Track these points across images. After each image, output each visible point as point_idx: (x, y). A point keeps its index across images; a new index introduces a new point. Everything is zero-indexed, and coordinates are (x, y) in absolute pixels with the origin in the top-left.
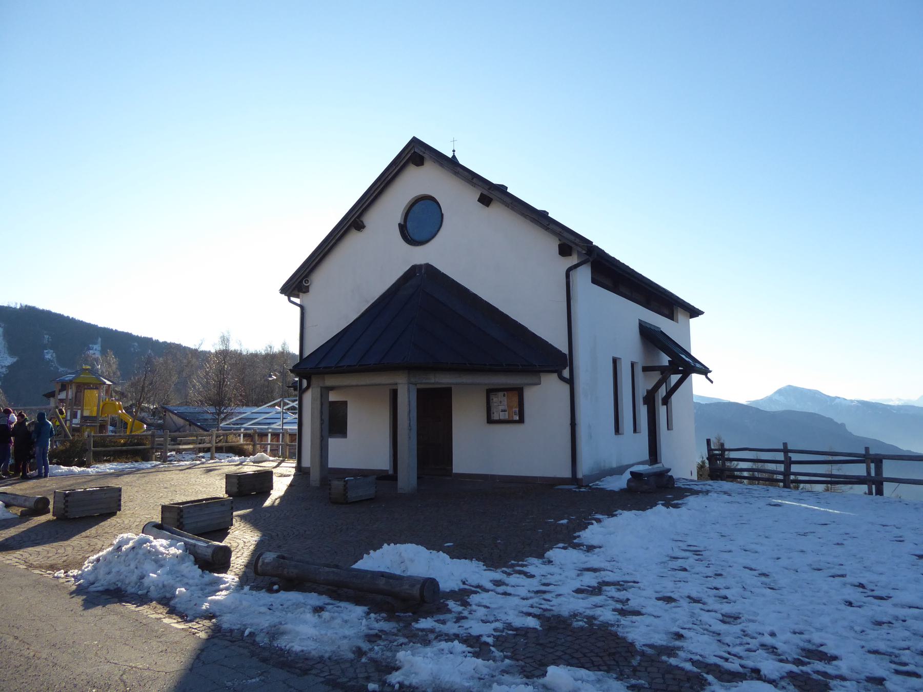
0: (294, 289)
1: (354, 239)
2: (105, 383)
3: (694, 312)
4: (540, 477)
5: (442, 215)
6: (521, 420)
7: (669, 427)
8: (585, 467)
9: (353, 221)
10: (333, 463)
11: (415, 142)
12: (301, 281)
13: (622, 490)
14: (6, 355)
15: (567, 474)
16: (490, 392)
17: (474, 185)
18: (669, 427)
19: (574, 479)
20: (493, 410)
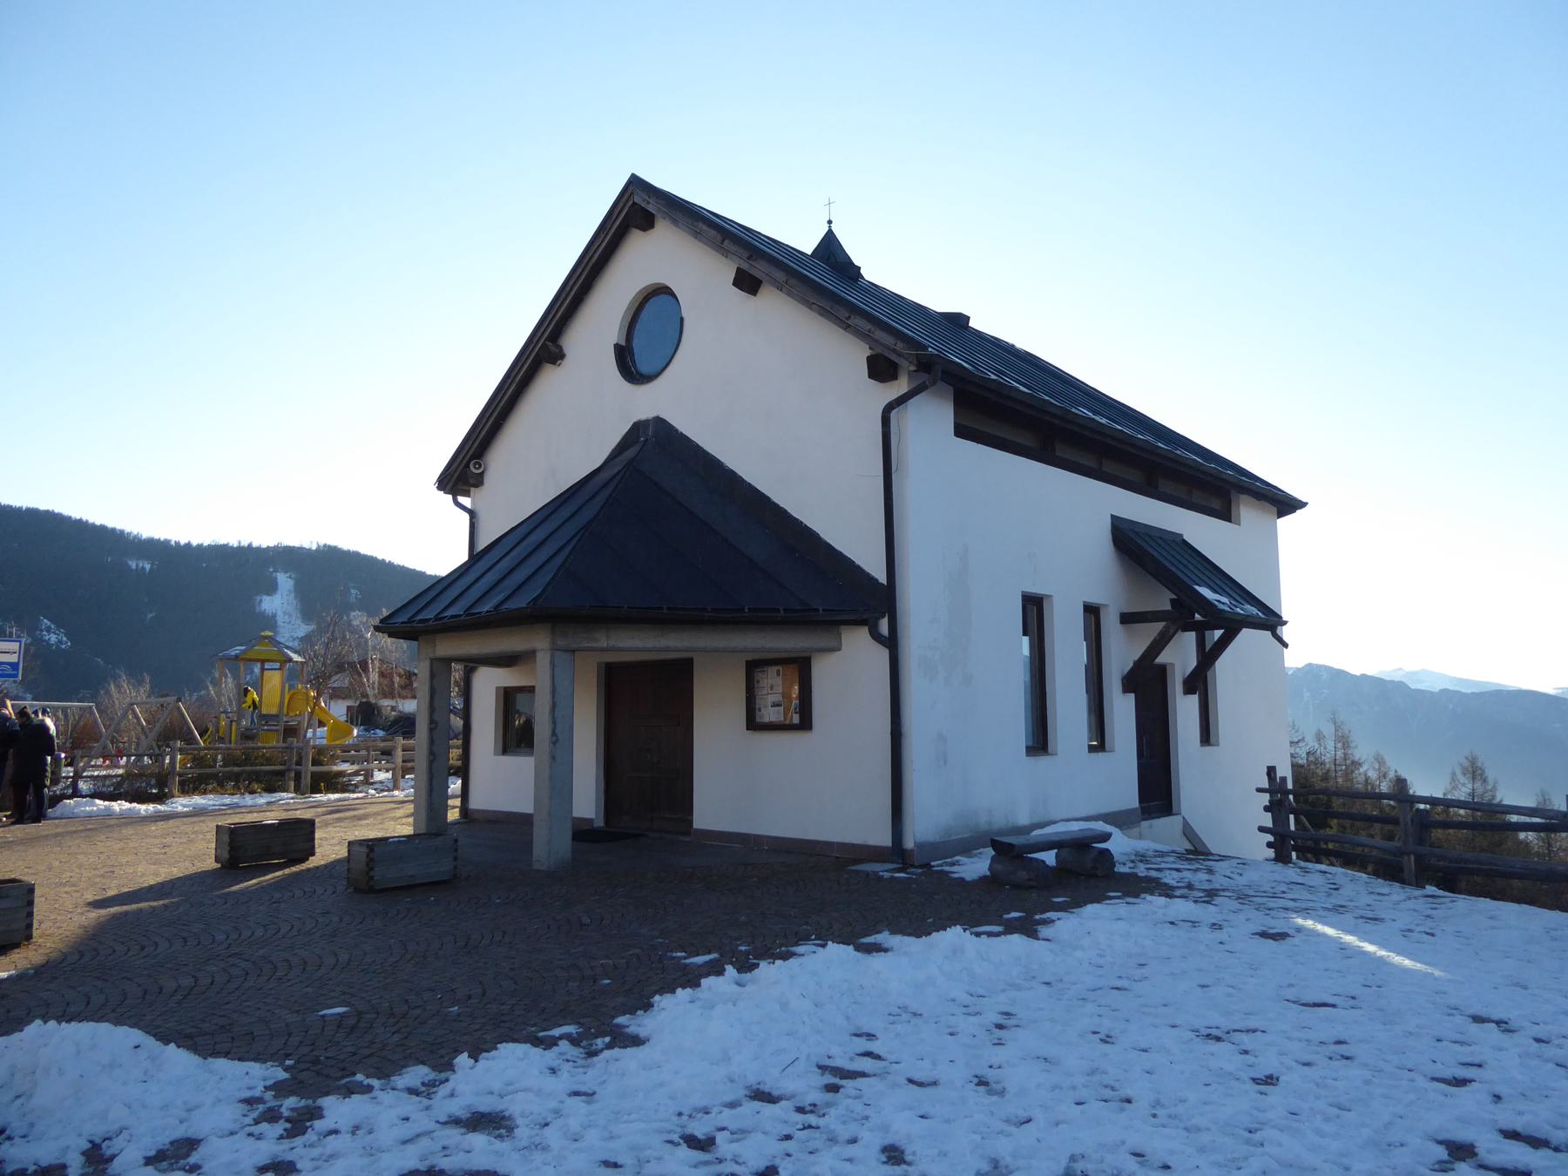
0: (456, 483)
1: (550, 381)
2: (290, 660)
3: (1286, 505)
4: (839, 844)
5: (682, 319)
6: (805, 724)
7: (1207, 736)
8: (923, 825)
9: (544, 348)
10: (475, 803)
11: (635, 183)
12: (467, 466)
13: (983, 879)
14: (299, 622)
15: (884, 839)
16: (754, 667)
17: (725, 253)
18: (1207, 736)
19: (897, 853)
20: (759, 702)
